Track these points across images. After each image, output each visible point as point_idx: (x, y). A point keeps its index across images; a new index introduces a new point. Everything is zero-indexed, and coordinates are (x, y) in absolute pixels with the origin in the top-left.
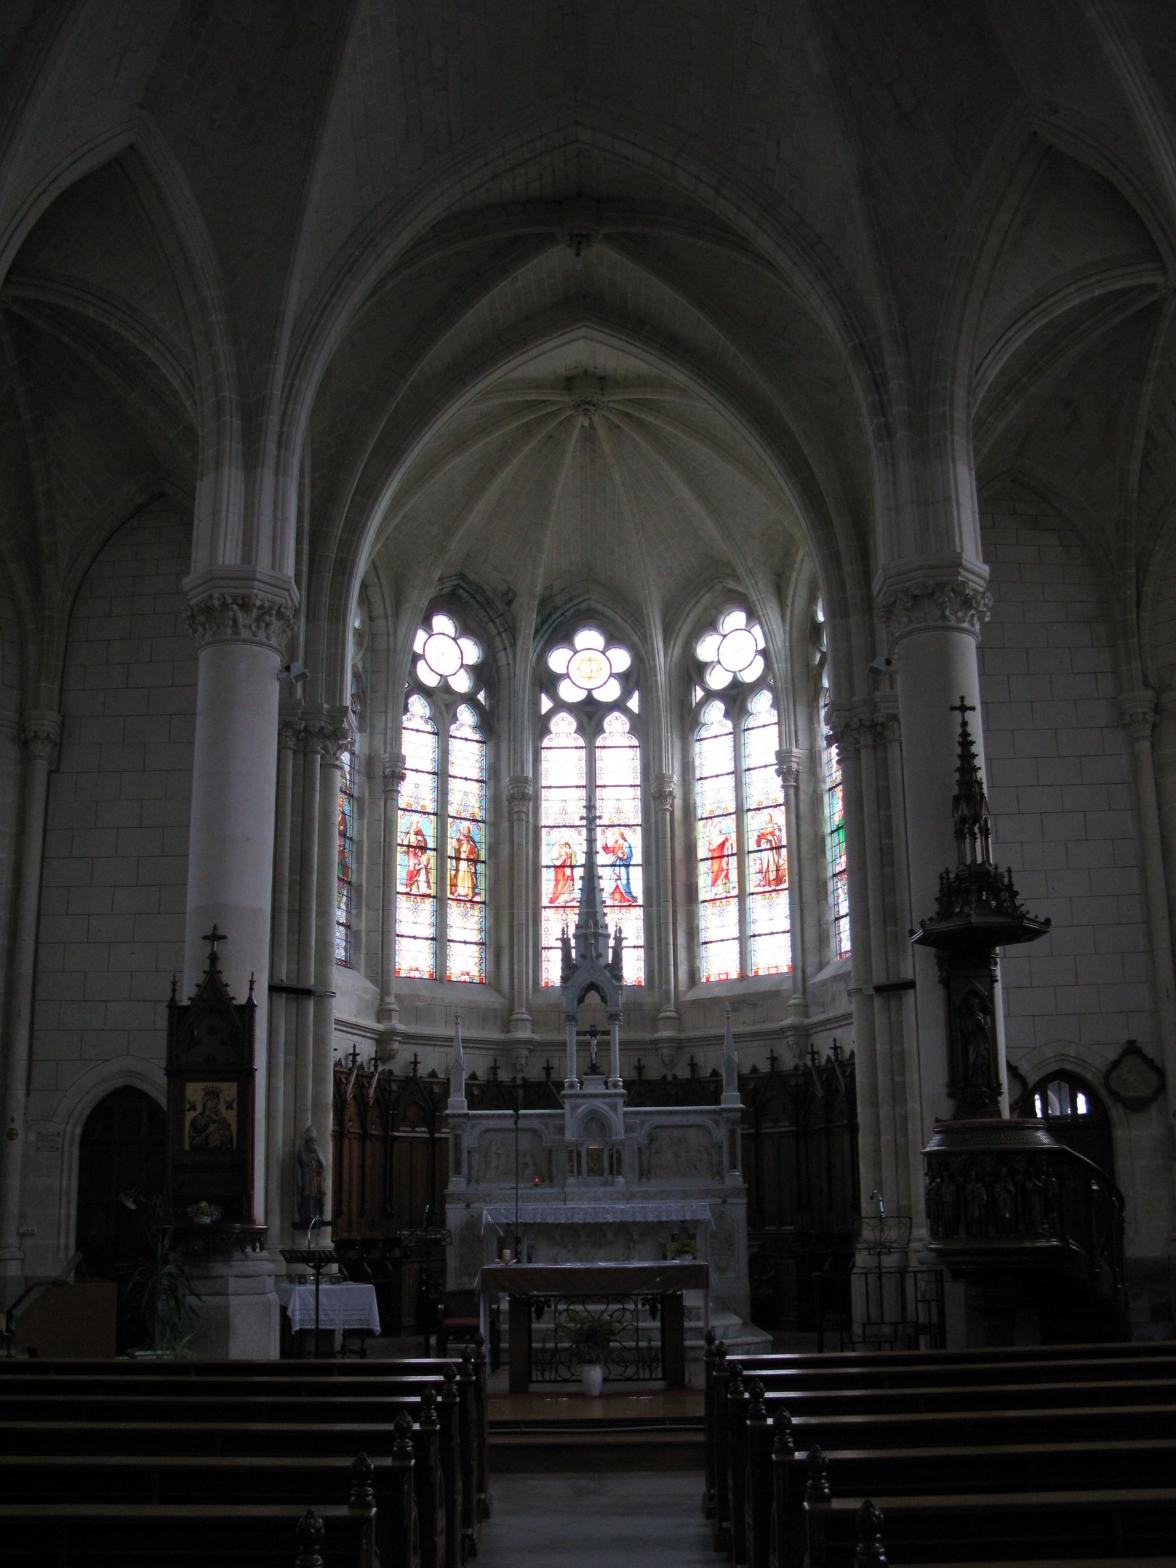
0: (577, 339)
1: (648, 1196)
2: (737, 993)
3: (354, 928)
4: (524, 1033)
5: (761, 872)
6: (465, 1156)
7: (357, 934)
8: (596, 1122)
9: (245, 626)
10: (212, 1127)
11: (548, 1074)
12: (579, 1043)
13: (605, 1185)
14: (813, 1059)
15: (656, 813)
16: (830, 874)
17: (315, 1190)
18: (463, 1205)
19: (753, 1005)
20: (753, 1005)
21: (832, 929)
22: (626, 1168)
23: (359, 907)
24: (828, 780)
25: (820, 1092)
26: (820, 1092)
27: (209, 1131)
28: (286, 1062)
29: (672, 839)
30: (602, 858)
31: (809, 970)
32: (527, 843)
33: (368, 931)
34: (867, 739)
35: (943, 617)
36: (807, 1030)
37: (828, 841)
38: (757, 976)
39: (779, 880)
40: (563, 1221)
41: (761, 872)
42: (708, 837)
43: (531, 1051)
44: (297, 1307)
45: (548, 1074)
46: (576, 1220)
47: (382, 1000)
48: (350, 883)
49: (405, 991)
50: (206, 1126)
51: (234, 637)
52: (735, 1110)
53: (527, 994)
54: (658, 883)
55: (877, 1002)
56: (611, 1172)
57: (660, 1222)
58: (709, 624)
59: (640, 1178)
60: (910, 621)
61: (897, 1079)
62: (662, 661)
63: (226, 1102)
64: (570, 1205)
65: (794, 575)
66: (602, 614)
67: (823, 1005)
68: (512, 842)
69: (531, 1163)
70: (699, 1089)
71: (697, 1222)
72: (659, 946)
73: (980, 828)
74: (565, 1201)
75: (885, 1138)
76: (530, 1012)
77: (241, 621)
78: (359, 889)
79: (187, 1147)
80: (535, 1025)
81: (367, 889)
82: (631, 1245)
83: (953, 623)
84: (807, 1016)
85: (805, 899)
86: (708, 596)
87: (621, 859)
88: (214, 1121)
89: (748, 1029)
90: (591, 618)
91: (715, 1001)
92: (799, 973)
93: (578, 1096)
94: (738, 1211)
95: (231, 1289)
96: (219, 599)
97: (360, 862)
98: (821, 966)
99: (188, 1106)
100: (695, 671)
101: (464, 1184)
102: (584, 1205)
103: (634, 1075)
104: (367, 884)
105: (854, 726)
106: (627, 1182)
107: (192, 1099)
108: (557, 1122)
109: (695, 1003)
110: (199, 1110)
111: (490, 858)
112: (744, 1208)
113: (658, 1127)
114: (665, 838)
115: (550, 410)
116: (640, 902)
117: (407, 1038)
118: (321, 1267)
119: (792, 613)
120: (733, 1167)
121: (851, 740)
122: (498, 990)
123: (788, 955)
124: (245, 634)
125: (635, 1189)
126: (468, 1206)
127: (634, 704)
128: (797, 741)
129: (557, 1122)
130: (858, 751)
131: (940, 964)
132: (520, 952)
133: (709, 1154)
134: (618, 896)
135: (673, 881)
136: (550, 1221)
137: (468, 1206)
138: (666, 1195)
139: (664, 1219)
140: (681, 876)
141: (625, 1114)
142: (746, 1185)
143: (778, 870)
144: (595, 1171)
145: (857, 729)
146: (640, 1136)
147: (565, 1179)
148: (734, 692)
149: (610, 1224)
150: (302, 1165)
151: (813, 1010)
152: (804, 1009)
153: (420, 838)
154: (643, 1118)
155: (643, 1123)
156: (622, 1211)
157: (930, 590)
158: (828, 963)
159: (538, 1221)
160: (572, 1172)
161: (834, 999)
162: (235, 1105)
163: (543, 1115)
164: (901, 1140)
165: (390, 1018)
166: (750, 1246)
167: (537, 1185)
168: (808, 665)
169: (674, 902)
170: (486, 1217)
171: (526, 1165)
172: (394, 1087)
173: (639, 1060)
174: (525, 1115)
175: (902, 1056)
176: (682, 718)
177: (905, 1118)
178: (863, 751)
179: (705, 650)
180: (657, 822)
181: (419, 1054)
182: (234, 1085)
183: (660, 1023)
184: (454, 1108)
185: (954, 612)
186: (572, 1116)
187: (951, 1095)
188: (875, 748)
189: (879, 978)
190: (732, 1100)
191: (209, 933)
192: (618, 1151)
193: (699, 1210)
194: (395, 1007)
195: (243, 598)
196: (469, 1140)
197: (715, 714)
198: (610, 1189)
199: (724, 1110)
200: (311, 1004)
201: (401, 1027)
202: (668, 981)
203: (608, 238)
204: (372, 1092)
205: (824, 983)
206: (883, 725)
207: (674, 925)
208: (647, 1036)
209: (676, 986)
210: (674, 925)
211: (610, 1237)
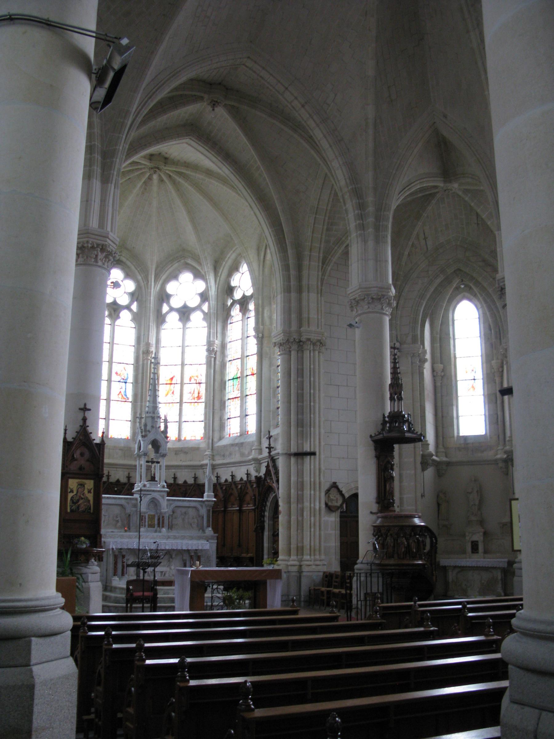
0: (183, 143)
5: (190, 393)
8: (154, 502)
9: (100, 259)
10: (81, 501)
11: (129, 480)
12: (147, 466)
13: (156, 531)
15: (143, 360)
19: (186, 453)
20: (186, 453)
21: (226, 422)
24: (229, 357)
27: (79, 503)
30: (114, 377)
31: (215, 440)
34: (295, 347)
35: (382, 309)
37: (227, 383)
38: (185, 440)
39: (199, 397)
41: (190, 393)
42: (164, 374)
45: (129, 480)
50: (78, 500)
51: (95, 263)
52: (212, 501)
54: (142, 392)
55: (293, 459)
58: (175, 277)
60: (369, 307)
61: (299, 493)
62: (154, 290)
63: (88, 489)
65: (224, 263)
66: (125, 263)
67: (224, 456)
70: (196, 489)
73: (397, 397)
77: (99, 257)
79: (69, 511)
82: (171, 560)
83: (384, 312)
84: (213, 460)
86: (177, 264)
87: (123, 379)
88: (82, 499)
89: (184, 464)
90: (119, 264)
94: (214, 546)
95: (90, 579)
96: (91, 244)
98: (221, 438)
99: (69, 490)
100: (164, 297)
103: (171, 481)
105: (291, 341)
107: (71, 487)
108: (134, 502)
110: (75, 493)
113: (176, 507)
114: (147, 372)
115: (140, 167)
116: (130, 400)
118: (146, 569)
119: (220, 280)
120: (208, 526)
121: (288, 346)
123: (203, 431)
124: (100, 263)
127: (134, 307)
128: (217, 337)
130: (290, 352)
131: (376, 450)
133: (198, 520)
134: (120, 396)
138: (183, 538)
143: (199, 393)
144: (151, 526)
145: (292, 342)
148: (185, 310)
151: (216, 458)
152: (213, 457)
154: (171, 502)
157: (379, 297)
162: (92, 491)
163: (127, 498)
164: (300, 519)
167: (126, 531)
168: (224, 304)
173: (129, 474)
174: (105, 497)
175: (302, 483)
176: (158, 317)
177: (302, 510)
178: (293, 353)
179: (171, 287)
180: (143, 364)
181: (197, 473)
182: (92, 482)
185: (386, 307)
187: (378, 503)
188: (298, 351)
189: (293, 450)
190: (208, 496)
191: (82, 406)
192: (163, 517)
195: (103, 245)
197: (173, 319)
199: (207, 501)
203: (225, 106)
206: (304, 342)
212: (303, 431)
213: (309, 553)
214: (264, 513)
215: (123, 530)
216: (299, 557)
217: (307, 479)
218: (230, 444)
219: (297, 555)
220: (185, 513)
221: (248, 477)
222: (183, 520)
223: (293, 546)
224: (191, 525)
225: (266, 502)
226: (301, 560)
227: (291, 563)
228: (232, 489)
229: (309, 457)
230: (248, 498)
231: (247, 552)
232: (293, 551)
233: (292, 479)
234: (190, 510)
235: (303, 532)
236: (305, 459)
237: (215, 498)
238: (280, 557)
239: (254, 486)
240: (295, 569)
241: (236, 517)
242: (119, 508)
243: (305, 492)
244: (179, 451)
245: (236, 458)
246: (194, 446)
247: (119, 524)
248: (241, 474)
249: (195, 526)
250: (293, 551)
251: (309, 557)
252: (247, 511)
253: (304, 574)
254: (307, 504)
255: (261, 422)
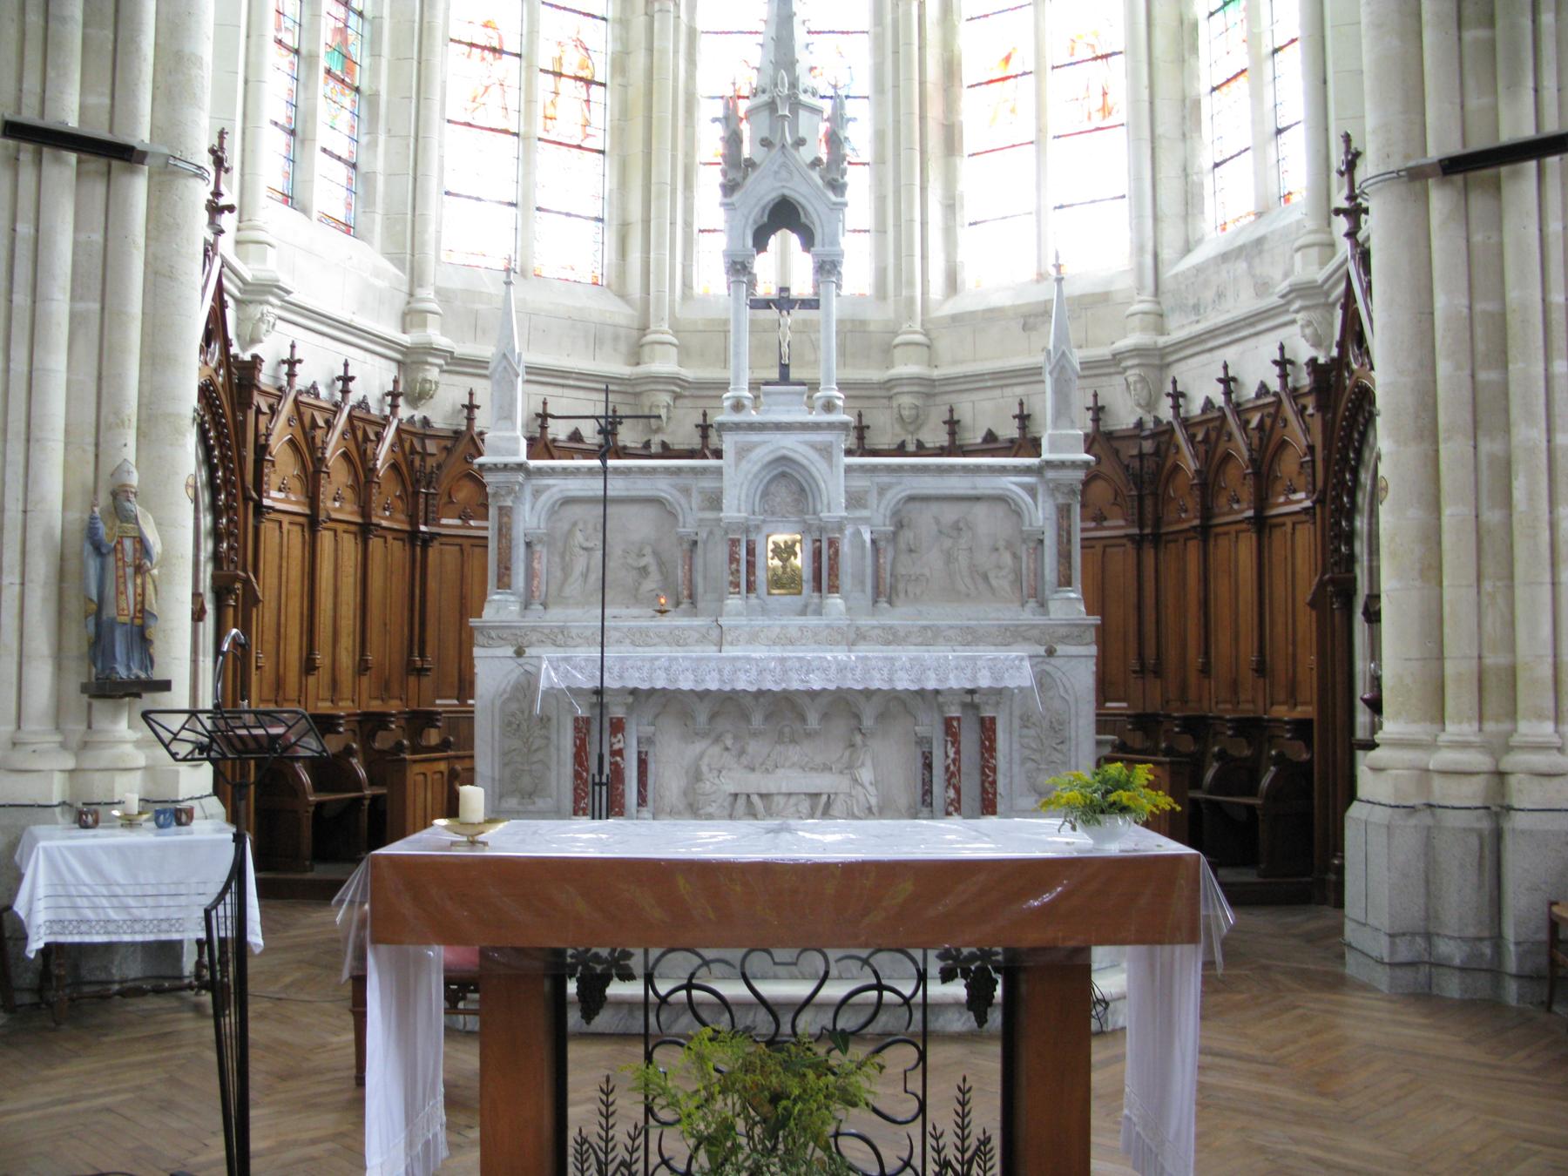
1: (892, 637)
2: (1033, 299)
3: (363, 168)
4: (663, 364)
6: (520, 552)
7: (368, 179)
8: (788, 483)
13: (803, 612)
14: (1176, 407)
16: (1204, 87)
17: (129, 603)
18: (510, 651)
22: (846, 580)
23: (373, 130)
25: (1189, 463)
26: (1189, 463)
28: (73, 316)
29: (921, 48)
31: (1166, 254)
32: (676, 52)
33: (389, 176)
36: (1162, 357)
40: (713, 687)
43: (677, 397)
44: (41, 891)
46: (741, 685)
47: (411, 295)
48: (357, 90)
49: (456, 283)
52: (1074, 465)
53: (672, 301)
54: (897, 122)
55: (1440, 199)
56: (818, 587)
57: (921, 693)
59: (875, 602)
61: (1483, 376)
64: (729, 651)
68: (650, 50)
69: (653, 568)
71: (999, 693)
72: (897, 226)
74: (720, 645)
75: (1451, 512)
76: (676, 333)
78: (373, 100)
80: (684, 353)
81: (388, 102)
82: (858, 739)
84: (1161, 331)
85: (1160, 130)
91: (992, 315)
92: (1149, 260)
93: (752, 427)
94: (1079, 671)
97: (375, 54)
98: (1187, 249)
101: (515, 608)
102: (759, 652)
104: (389, 93)
106: (849, 609)
109: (956, 319)
111: (612, 77)
112: (1091, 666)
113: (912, 499)
117: (457, 364)
120: (1065, 581)
122: (622, 295)
125: (864, 621)
126: (519, 653)
129: (707, 483)
132: (660, 235)
133: (1015, 556)
135: (922, 118)
136: (686, 685)
137: (519, 653)
138: (930, 636)
139: (931, 685)
140: (935, 111)
141: (849, 469)
142: (1095, 620)
146: (878, 515)
147: (721, 600)
149: (813, 694)
150: (98, 548)
152: (1158, 320)
153: (490, 31)
154: (885, 479)
155: (882, 491)
156: (842, 668)
158: (1200, 241)
159: (659, 685)
160: (737, 585)
161: (1220, 295)
163: (679, 471)
164: (1492, 516)
165: (424, 325)
166: (1099, 743)
169: (923, 152)
170: (549, 678)
171: (644, 571)
172: (431, 447)
175: (1500, 323)
177: (1505, 468)
183: (897, 352)
184: (497, 452)
186: (738, 478)
193: (1008, 667)
194: (434, 306)
196: (528, 518)
198: (812, 621)
199: (1050, 464)
200: (139, 187)
201: (442, 341)
202: (911, 284)
204: (383, 451)
205: (1199, 269)
207: (923, 189)
208: (875, 375)
209: (924, 293)
210: (923, 189)
211: (813, 721)
212: (1492, 44)
213: (1549, 703)
214: (1351, 521)
215: (651, 612)
216: (1490, 726)
217: (1523, 292)
218: (1215, 258)
219: (1481, 719)
220: (956, 527)
221: (1283, 376)
222: (949, 558)
223: (1457, 666)
224: (986, 578)
225: (1355, 473)
226: (1506, 747)
227: (1446, 758)
228: (1230, 436)
229: (1532, 165)
230: (1289, 465)
231: (1293, 700)
232: (1458, 698)
233: (1440, 301)
234: (980, 510)
235: (1511, 588)
236: (1508, 190)
237: (1087, 452)
238: (1391, 727)
239: (1310, 411)
240: (1470, 792)
241: (1245, 550)
242: (650, 512)
243: (1515, 367)
244: (1036, 316)
245: (1243, 303)
246: (1089, 289)
247: (651, 584)
248: (1256, 368)
249: (1002, 582)
250: (1458, 698)
251: (1548, 727)
252: (1289, 521)
253: (1519, 821)
254: (1528, 434)
255: (1327, 130)
